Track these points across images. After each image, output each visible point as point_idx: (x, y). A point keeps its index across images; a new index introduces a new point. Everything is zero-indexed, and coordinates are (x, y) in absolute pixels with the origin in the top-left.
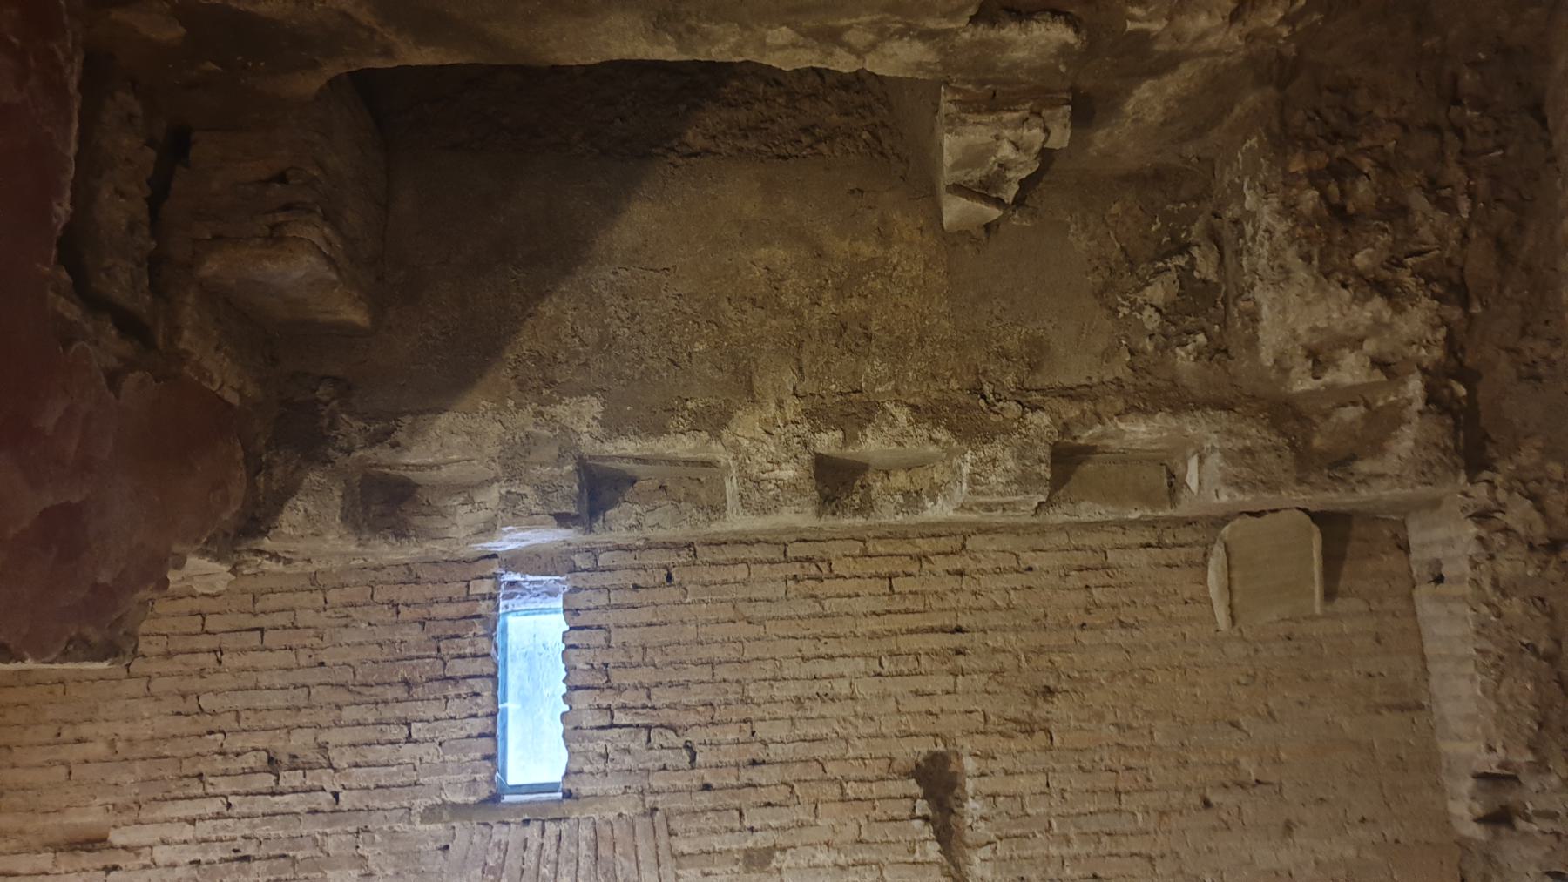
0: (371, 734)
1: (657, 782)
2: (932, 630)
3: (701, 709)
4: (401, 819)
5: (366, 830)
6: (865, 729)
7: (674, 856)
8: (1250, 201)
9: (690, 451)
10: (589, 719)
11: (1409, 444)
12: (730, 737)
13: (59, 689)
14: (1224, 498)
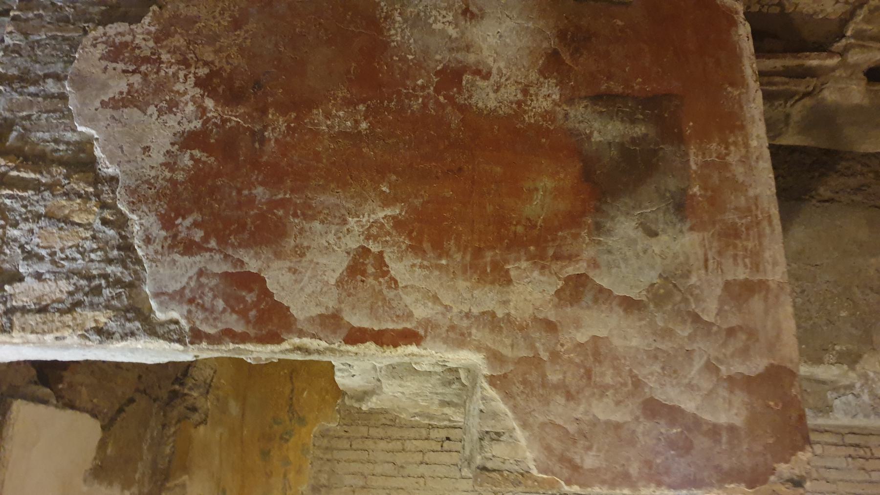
9: (835, 376)
13: (421, 481)
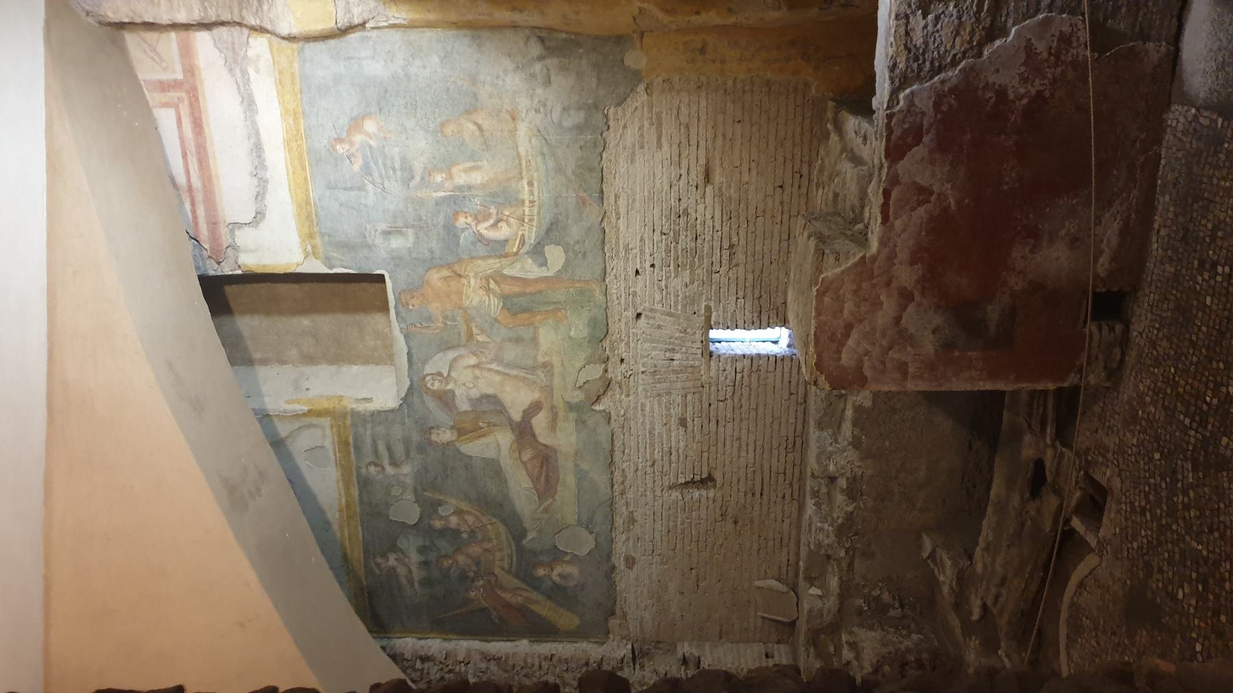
0: (741, 285)
2: (762, 489)
4: (707, 298)
8: (914, 637)
10: (739, 366)
12: (728, 414)
13: (773, 159)
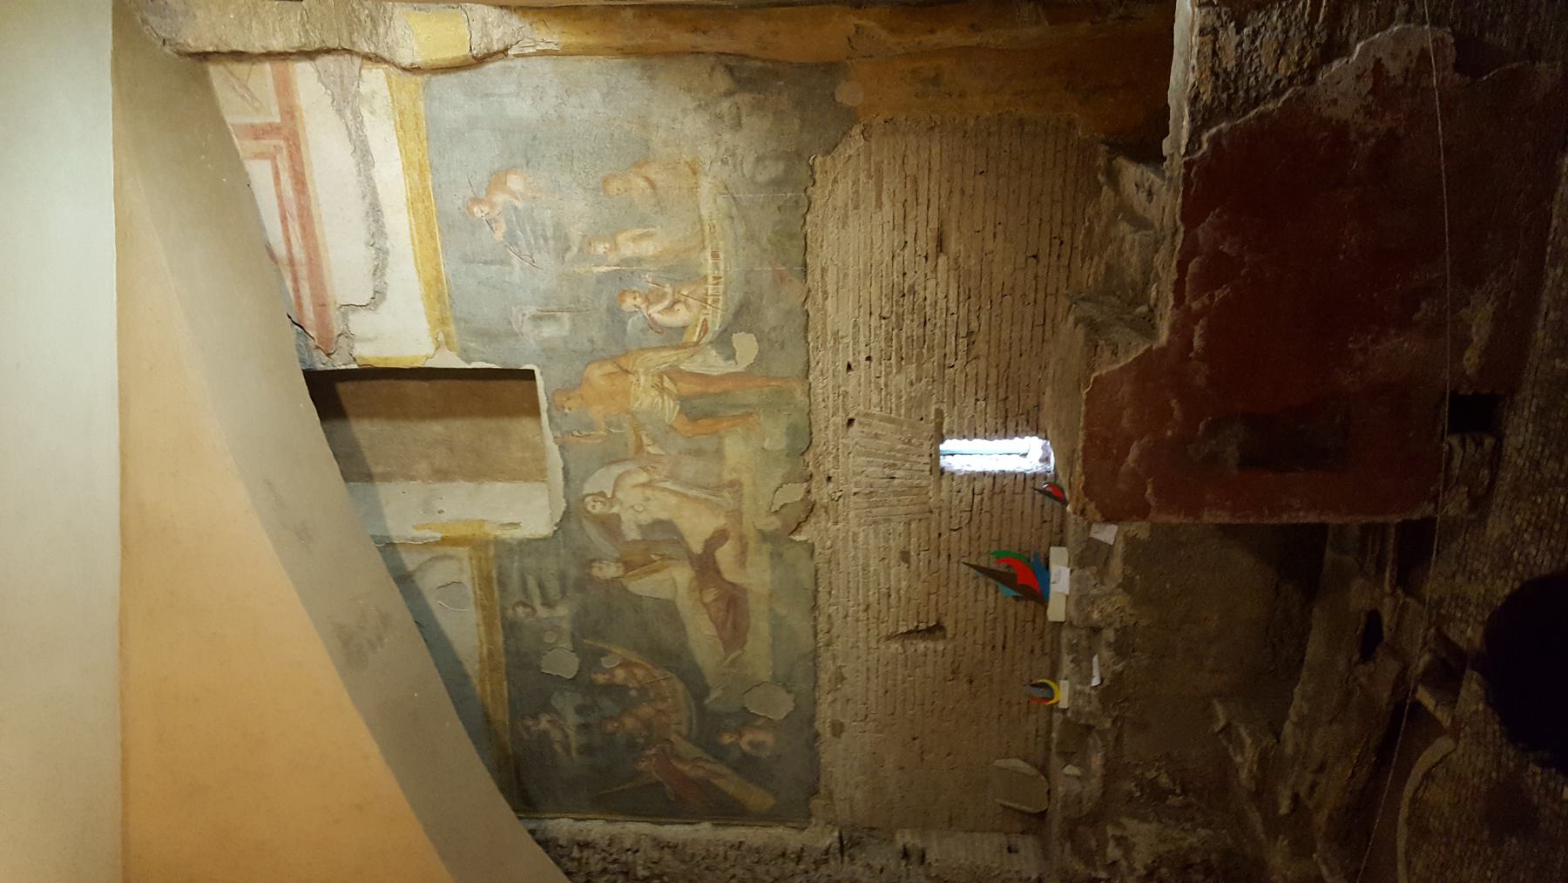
0: (982, 383)
1: (944, 514)
2: (1005, 637)
3: (978, 534)
5: (934, 381)
6: (961, 605)
7: (910, 520)
8: (1202, 832)
11: (1077, 867)
13: (1025, 221)
14: (1060, 789)
